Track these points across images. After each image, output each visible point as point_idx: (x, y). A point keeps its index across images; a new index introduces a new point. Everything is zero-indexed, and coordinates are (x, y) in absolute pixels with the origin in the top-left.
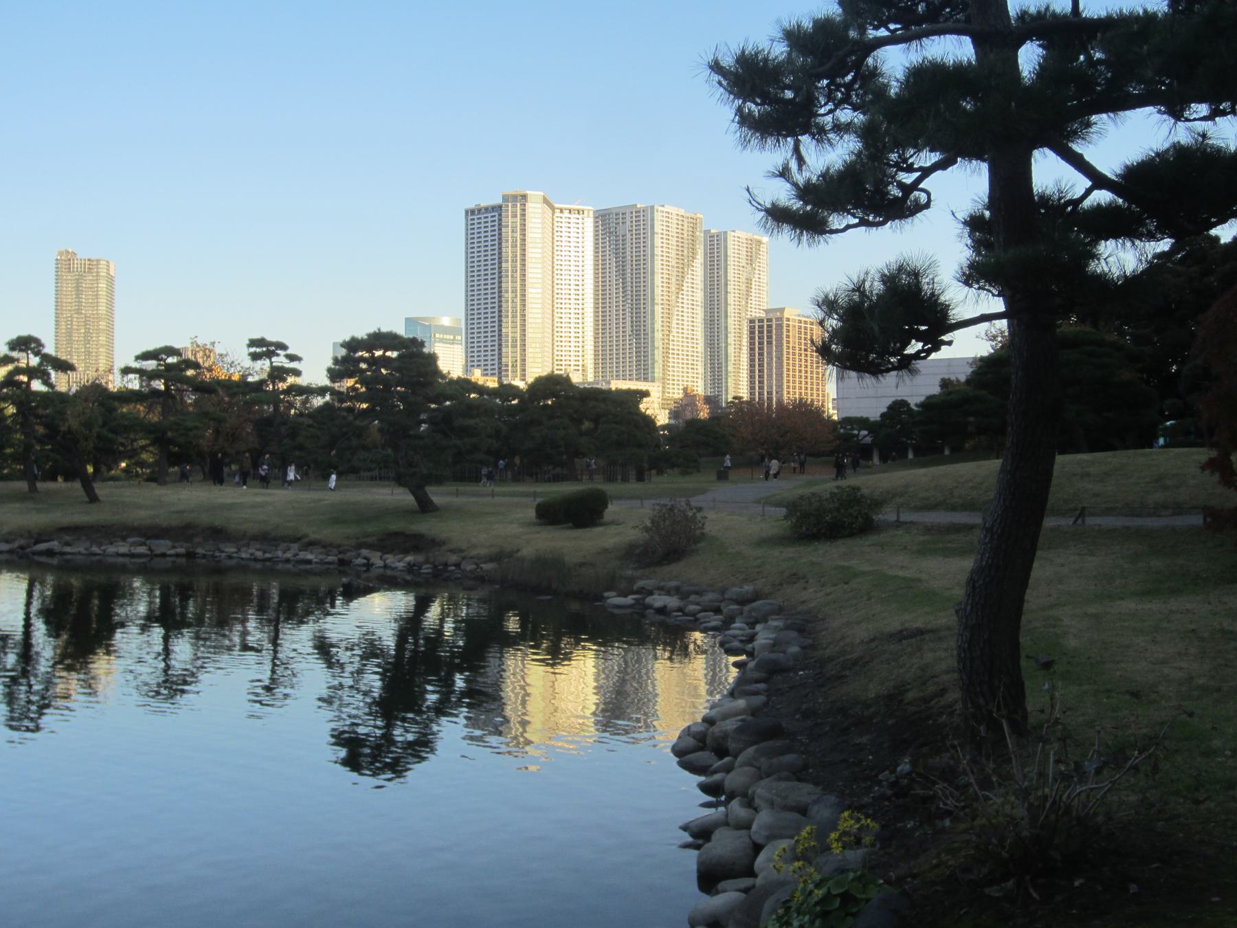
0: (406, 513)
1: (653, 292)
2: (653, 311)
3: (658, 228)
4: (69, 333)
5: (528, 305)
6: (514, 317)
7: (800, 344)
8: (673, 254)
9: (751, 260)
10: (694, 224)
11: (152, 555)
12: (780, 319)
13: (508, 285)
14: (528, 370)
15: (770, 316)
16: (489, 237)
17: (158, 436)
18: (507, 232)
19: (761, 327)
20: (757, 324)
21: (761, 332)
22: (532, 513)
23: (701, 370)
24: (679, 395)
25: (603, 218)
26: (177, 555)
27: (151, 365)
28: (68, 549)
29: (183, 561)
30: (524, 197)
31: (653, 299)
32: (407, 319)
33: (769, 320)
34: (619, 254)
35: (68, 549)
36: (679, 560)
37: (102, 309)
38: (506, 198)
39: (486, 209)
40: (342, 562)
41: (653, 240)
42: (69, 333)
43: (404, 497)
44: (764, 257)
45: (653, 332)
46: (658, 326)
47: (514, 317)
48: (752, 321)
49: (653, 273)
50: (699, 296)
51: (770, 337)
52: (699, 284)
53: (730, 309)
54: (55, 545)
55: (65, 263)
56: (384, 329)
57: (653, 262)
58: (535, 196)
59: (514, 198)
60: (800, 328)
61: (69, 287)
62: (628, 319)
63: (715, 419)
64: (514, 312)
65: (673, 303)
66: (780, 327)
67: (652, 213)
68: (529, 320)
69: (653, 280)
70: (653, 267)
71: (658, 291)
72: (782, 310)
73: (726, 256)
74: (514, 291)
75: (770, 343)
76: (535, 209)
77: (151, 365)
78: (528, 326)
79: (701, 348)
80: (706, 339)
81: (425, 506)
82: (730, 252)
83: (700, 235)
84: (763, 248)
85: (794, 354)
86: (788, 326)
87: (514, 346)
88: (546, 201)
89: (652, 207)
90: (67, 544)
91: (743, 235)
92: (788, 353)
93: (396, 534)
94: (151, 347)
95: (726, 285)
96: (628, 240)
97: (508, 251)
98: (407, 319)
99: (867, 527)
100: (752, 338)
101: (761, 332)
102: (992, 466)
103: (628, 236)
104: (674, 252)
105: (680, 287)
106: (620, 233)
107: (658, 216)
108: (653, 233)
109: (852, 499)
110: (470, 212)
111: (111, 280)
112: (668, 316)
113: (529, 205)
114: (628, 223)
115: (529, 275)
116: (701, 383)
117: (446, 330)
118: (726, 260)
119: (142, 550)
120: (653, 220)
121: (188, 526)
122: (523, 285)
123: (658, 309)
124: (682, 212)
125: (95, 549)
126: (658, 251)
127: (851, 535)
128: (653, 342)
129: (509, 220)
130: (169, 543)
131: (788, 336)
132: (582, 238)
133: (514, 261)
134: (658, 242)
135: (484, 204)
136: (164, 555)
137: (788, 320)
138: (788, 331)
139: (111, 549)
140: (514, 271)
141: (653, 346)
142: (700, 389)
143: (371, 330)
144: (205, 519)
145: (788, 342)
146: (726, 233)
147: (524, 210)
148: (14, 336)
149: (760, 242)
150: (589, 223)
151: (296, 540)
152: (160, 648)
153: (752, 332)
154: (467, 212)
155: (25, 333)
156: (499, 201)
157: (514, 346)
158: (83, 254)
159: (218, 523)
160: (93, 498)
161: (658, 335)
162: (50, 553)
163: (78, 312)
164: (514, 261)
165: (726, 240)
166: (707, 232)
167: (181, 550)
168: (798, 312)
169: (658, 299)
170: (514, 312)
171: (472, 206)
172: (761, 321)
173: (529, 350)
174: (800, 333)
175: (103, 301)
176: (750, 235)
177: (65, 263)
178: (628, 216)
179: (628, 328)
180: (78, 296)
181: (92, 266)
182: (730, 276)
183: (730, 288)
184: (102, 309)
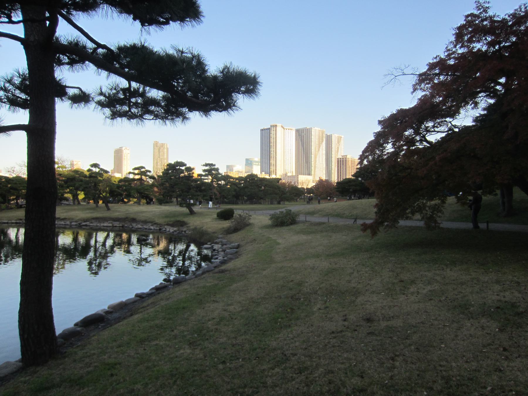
0: (186, 215)
3: (313, 134)
4: (157, 163)
8: (317, 141)
9: (339, 142)
11: (113, 226)
13: (272, 149)
14: (277, 172)
16: (267, 137)
17: (139, 192)
18: (272, 135)
22: (215, 216)
23: (325, 172)
24: (318, 179)
25: (297, 131)
26: (120, 226)
27: (136, 172)
28: (91, 224)
29: (121, 228)
30: (276, 126)
35: (91, 224)
36: (237, 232)
37: (165, 157)
38: (271, 126)
39: (266, 129)
40: (160, 229)
42: (157, 163)
43: (185, 210)
44: (342, 142)
46: (313, 160)
50: (324, 152)
53: (333, 156)
54: (88, 223)
55: (156, 144)
56: (179, 161)
58: (279, 125)
59: (274, 126)
61: (157, 151)
66: (346, 160)
71: (313, 151)
72: (346, 156)
76: (279, 129)
77: (136, 172)
79: (325, 166)
81: (192, 213)
83: (324, 135)
84: (342, 139)
88: (282, 127)
90: (92, 223)
91: (337, 135)
93: (178, 221)
94: (137, 166)
97: (272, 140)
99: (293, 222)
102: (373, 201)
105: (319, 150)
107: (313, 130)
109: (289, 213)
110: (262, 130)
111: (167, 149)
113: (278, 128)
116: (325, 176)
117: (256, 162)
119: (110, 225)
121: (127, 218)
123: (313, 156)
125: (99, 225)
126: (313, 140)
127: (288, 225)
130: (118, 223)
132: (292, 136)
134: (313, 137)
135: (265, 128)
136: (116, 226)
139: (102, 225)
142: (324, 178)
143: (175, 161)
144: (132, 216)
148: (92, 163)
150: (294, 133)
151: (149, 222)
152: (139, 251)
153: (338, 162)
155: (95, 162)
158: (160, 142)
159: (135, 217)
160: (108, 209)
161: (313, 163)
162: (86, 225)
163: (159, 157)
166: (326, 135)
167: (121, 225)
169: (313, 153)
173: (277, 167)
175: (165, 154)
177: (156, 144)
180: (159, 153)
181: (163, 145)
182: (333, 146)
184: (165, 157)
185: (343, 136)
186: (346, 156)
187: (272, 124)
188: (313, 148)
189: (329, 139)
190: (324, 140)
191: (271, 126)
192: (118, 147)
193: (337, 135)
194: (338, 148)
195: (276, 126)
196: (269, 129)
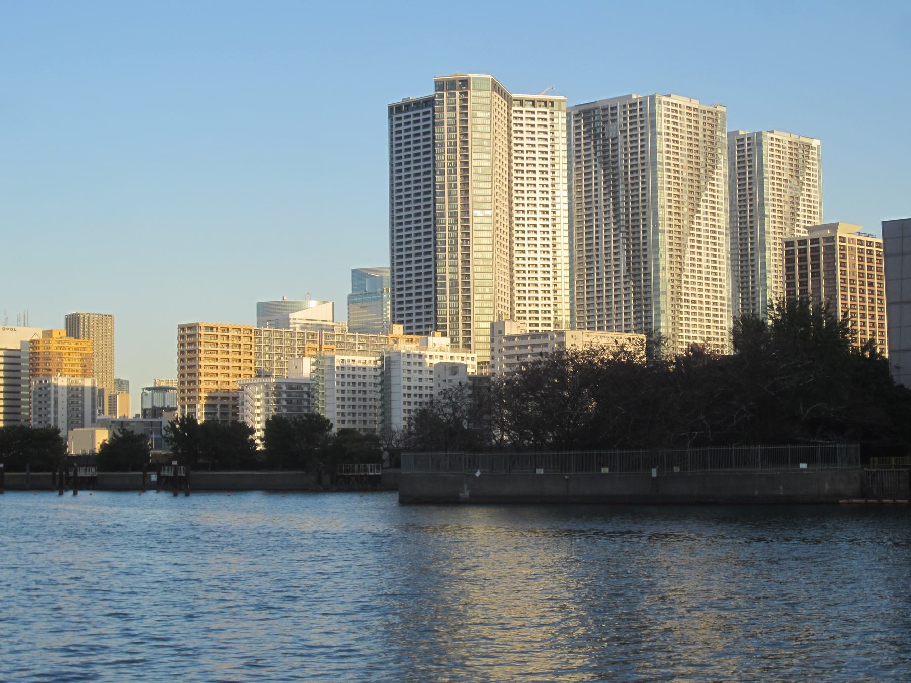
1: (656, 213)
2: (656, 242)
3: (661, 127)
5: (473, 234)
6: (454, 250)
7: (862, 275)
8: (684, 162)
10: (713, 121)
12: (831, 239)
15: (817, 235)
19: (803, 252)
20: (796, 247)
21: (803, 259)
31: (656, 224)
32: (354, 271)
33: (815, 241)
34: (608, 163)
38: (440, 86)
41: (654, 142)
44: (814, 167)
45: (657, 270)
46: (664, 262)
47: (454, 250)
48: (789, 244)
49: (655, 189)
50: (723, 220)
51: (816, 266)
52: (722, 203)
57: (655, 172)
59: (452, 85)
60: (861, 251)
62: (623, 254)
63: (60, 439)
64: (453, 244)
65: (686, 230)
66: (831, 250)
67: (653, 105)
68: (475, 255)
69: (655, 197)
70: (655, 179)
71: (663, 213)
72: (834, 227)
73: (761, 165)
74: (453, 215)
75: (816, 274)
76: (478, 97)
78: (473, 262)
80: (734, 277)
82: (767, 161)
85: (853, 290)
86: (843, 248)
87: (454, 292)
88: (496, 88)
89: (653, 98)
92: (844, 289)
95: (762, 205)
96: (621, 144)
98: (354, 271)
100: (790, 269)
101: (803, 259)
103: (621, 138)
104: (685, 159)
105: (694, 209)
106: (610, 134)
107: (661, 109)
108: (654, 134)
110: (395, 110)
112: (679, 248)
113: (472, 93)
114: (620, 121)
115: (473, 192)
118: (761, 172)
120: (653, 114)
122: (466, 206)
123: (664, 238)
124: (695, 104)
126: (661, 158)
128: (657, 284)
129: (446, 116)
131: (843, 264)
132: (551, 147)
133: (452, 172)
134: (661, 145)
135: (413, 97)
137: (843, 240)
138: (843, 256)
140: (453, 186)
141: (657, 290)
145: (844, 273)
146: (759, 134)
147: (465, 100)
149: (809, 146)
150: (561, 119)
153: (789, 260)
154: (391, 109)
156: (430, 92)
157: (454, 292)
161: (665, 275)
164: (452, 172)
165: (760, 144)
168: (859, 229)
169: (664, 225)
170: (453, 244)
171: (398, 100)
172: (802, 242)
173: (475, 297)
174: (861, 259)
176: (794, 138)
178: (619, 111)
179: (623, 267)
183: (768, 210)
185: (816, 143)
186: (834, 227)
187: (446, 75)
188: (663, 198)
189: (746, 157)
190: (723, 168)
191: (440, 86)
192: (49, 329)
193: (784, 136)
194: (794, 201)
195: (465, 82)
196: (429, 102)
